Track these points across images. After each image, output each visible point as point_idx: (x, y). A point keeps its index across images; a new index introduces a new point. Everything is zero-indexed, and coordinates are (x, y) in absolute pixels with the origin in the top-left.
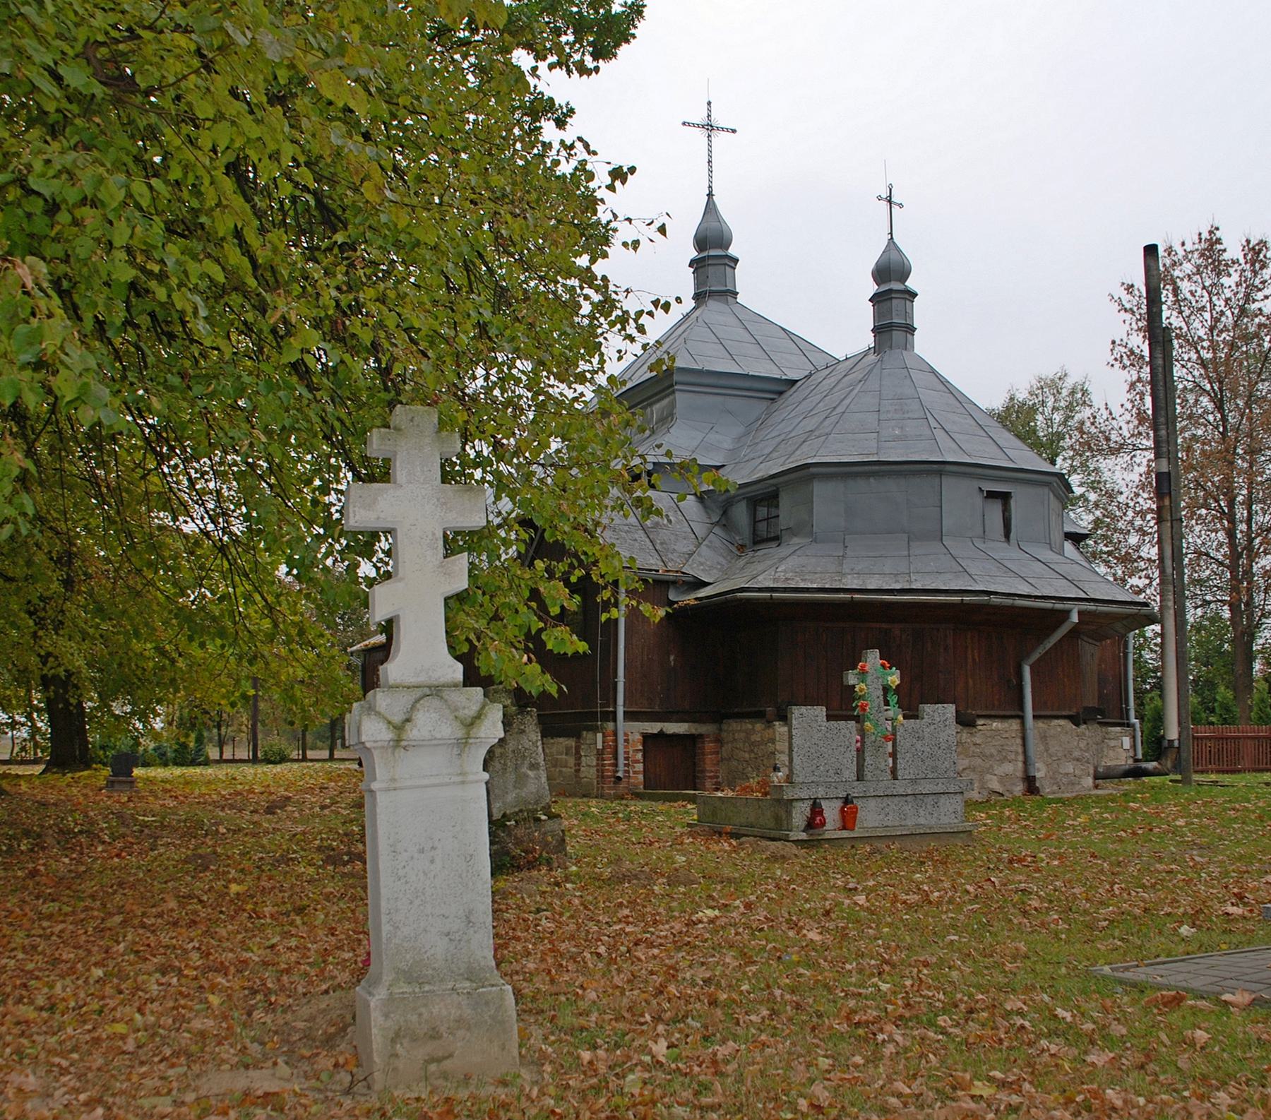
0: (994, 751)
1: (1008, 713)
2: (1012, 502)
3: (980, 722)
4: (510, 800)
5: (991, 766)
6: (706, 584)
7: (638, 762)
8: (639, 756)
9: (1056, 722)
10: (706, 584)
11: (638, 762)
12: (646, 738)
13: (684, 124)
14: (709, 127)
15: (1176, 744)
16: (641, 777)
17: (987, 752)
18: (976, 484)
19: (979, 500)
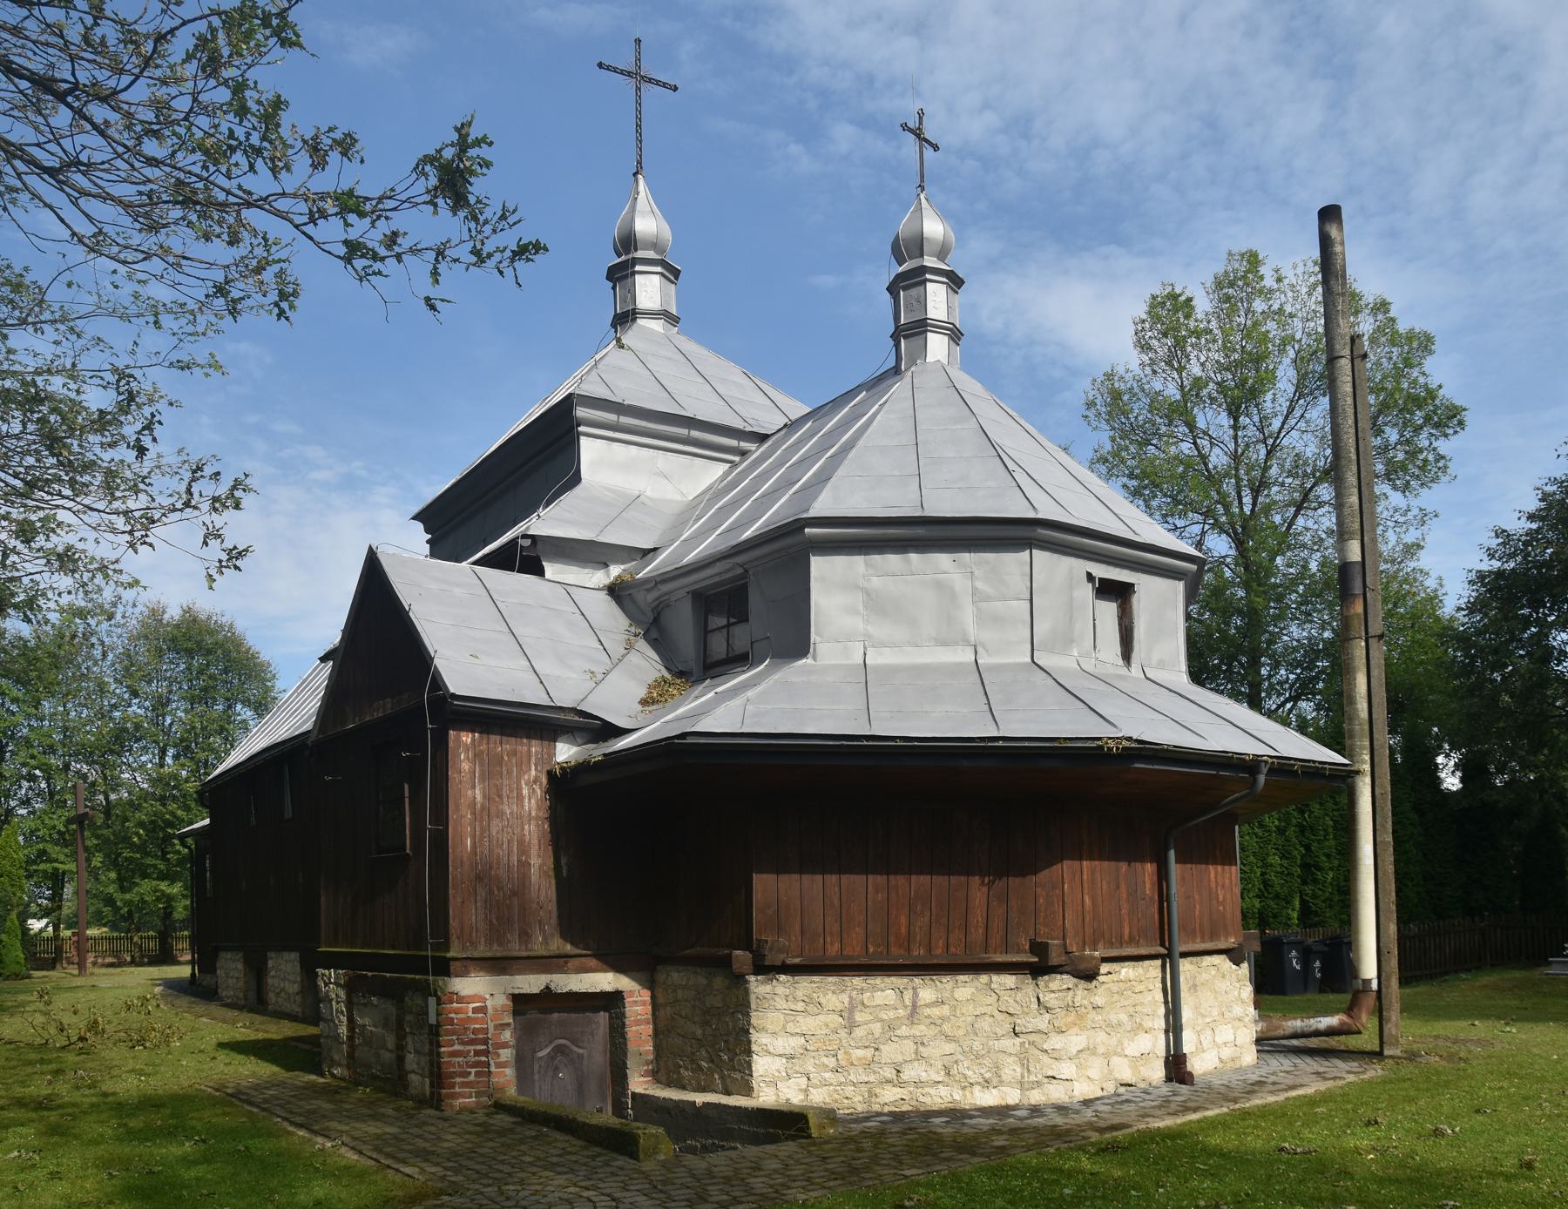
0: (1124, 1017)
1: (1143, 951)
2: (1135, 599)
3: (1104, 968)
4: (812, 1121)
5: (1120, 1042)
6: (622, 732)
7: (505, 1045)
8: (507, 1035)
9: (1208, 960)
10: (622, 732)
11: (505, 1045)
12: (520, 1002)
13: (600, 65)
14: (637, 76)
15: (1375, 985)
16: (509, 1072)
17: (1113, 1018)
18: (1084, 566)
19: (1088, 590)
